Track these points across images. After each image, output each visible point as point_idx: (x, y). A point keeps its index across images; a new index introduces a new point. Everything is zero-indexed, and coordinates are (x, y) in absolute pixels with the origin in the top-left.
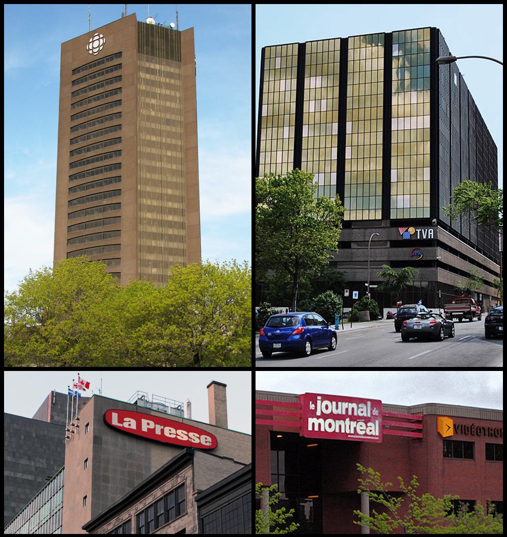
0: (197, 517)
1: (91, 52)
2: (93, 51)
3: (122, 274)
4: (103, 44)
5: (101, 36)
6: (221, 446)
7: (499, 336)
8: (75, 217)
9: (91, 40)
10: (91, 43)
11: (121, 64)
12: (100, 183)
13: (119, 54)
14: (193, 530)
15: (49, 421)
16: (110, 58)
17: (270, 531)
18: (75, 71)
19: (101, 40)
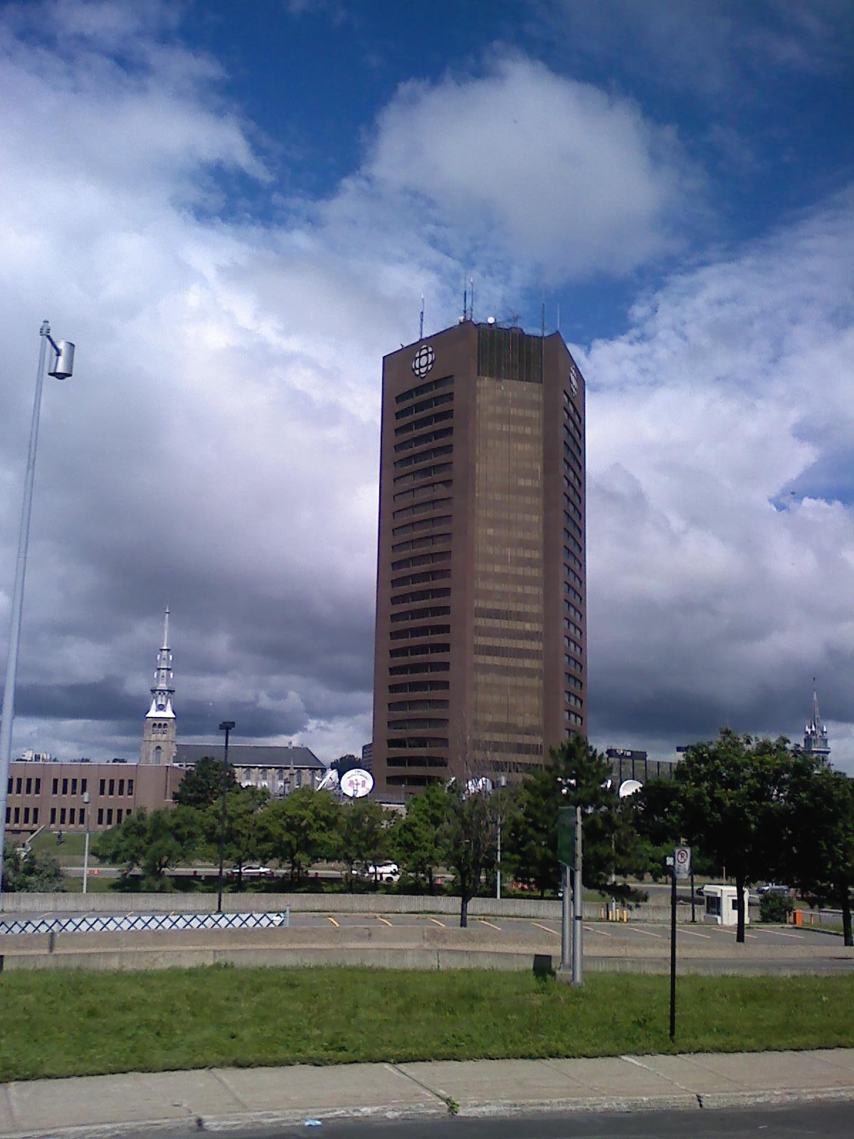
0: (830, 1095)
1: (417, 372)
2: (420, 372)
3: (451, 609)
4: (432, 362)
5: (430, 349)
6: (207, 1124)
7: (444, 924)
8: (399, 603)
9: (417, 355)
10: (418, 359)
11: (452, 393)
12: (425, 454)
13: (448, 379)
14: (338, 851)
15: (813, 749)
16: (437, 383)
17: (704, 904)
18: (399, 399)
19: (430, 355)
